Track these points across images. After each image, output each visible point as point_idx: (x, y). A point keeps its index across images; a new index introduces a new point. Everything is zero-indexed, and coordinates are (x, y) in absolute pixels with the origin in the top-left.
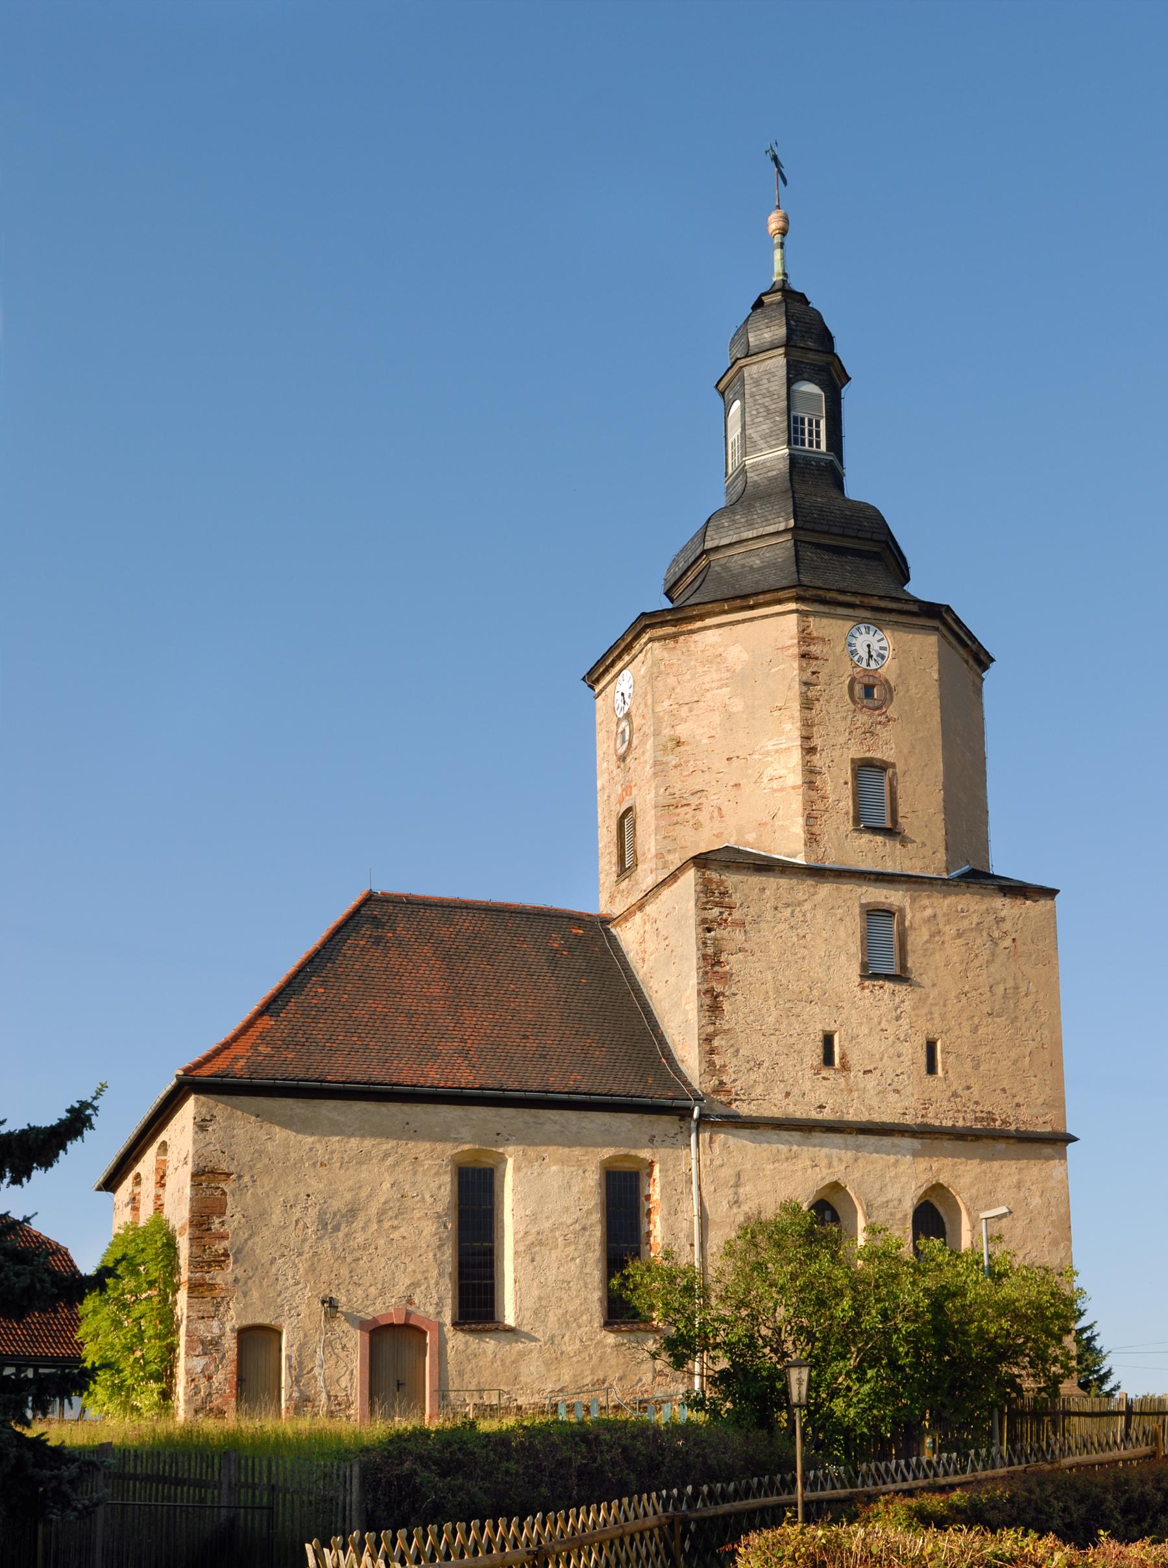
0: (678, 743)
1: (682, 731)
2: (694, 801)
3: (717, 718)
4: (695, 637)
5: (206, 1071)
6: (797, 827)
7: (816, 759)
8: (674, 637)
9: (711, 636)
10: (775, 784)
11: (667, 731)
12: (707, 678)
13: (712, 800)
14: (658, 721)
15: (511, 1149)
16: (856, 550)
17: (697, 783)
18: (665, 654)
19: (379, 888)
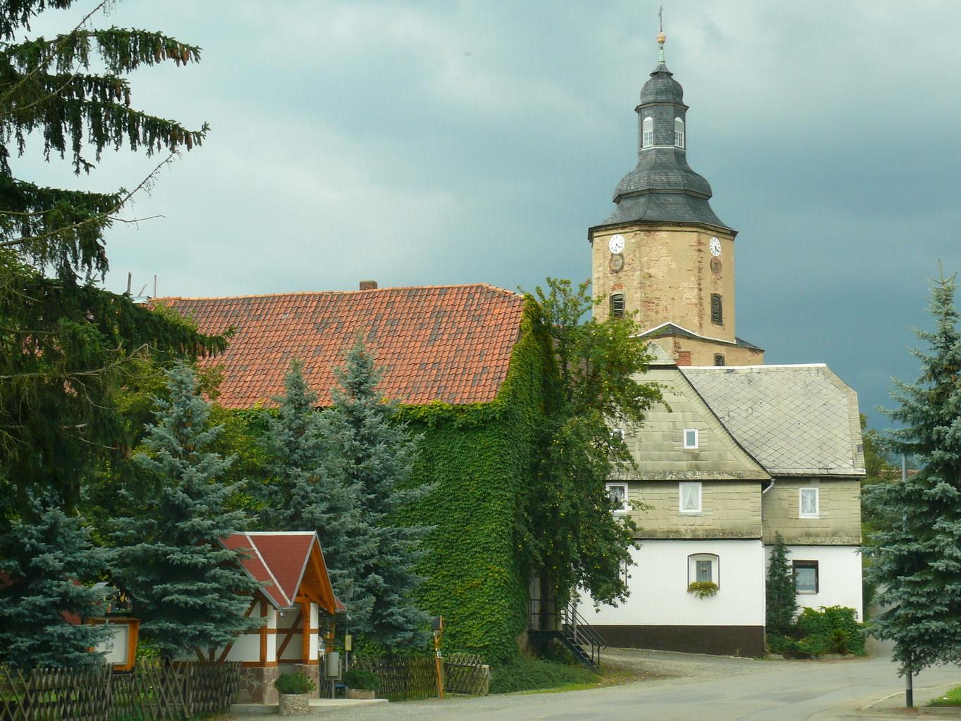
0: (650, 276)
1: (652, 271)
2: (656, 302)
3: (666, 269)
4: (658, 233)
5: (578, 616)
6: (696, 321)
7: (701, 293)
8: (649, 231)
9: (664, 234)
10: (688, 301)
11: (646, 270)
12: (662, 251)
13: (663, 303)
14: (642, 265)
15: (788, 556)
16: (683, 226)
17: (658, 294)
18: (645, 238)
19: (723, 299)
